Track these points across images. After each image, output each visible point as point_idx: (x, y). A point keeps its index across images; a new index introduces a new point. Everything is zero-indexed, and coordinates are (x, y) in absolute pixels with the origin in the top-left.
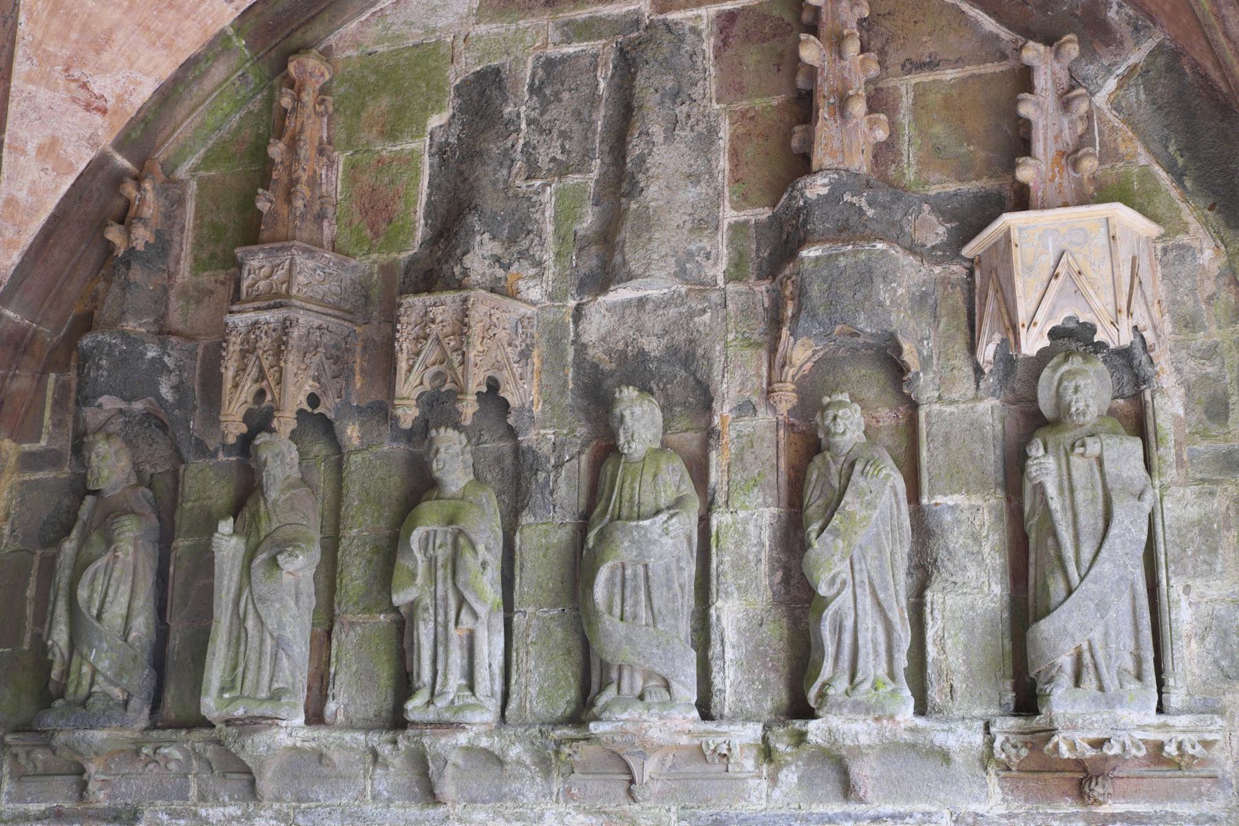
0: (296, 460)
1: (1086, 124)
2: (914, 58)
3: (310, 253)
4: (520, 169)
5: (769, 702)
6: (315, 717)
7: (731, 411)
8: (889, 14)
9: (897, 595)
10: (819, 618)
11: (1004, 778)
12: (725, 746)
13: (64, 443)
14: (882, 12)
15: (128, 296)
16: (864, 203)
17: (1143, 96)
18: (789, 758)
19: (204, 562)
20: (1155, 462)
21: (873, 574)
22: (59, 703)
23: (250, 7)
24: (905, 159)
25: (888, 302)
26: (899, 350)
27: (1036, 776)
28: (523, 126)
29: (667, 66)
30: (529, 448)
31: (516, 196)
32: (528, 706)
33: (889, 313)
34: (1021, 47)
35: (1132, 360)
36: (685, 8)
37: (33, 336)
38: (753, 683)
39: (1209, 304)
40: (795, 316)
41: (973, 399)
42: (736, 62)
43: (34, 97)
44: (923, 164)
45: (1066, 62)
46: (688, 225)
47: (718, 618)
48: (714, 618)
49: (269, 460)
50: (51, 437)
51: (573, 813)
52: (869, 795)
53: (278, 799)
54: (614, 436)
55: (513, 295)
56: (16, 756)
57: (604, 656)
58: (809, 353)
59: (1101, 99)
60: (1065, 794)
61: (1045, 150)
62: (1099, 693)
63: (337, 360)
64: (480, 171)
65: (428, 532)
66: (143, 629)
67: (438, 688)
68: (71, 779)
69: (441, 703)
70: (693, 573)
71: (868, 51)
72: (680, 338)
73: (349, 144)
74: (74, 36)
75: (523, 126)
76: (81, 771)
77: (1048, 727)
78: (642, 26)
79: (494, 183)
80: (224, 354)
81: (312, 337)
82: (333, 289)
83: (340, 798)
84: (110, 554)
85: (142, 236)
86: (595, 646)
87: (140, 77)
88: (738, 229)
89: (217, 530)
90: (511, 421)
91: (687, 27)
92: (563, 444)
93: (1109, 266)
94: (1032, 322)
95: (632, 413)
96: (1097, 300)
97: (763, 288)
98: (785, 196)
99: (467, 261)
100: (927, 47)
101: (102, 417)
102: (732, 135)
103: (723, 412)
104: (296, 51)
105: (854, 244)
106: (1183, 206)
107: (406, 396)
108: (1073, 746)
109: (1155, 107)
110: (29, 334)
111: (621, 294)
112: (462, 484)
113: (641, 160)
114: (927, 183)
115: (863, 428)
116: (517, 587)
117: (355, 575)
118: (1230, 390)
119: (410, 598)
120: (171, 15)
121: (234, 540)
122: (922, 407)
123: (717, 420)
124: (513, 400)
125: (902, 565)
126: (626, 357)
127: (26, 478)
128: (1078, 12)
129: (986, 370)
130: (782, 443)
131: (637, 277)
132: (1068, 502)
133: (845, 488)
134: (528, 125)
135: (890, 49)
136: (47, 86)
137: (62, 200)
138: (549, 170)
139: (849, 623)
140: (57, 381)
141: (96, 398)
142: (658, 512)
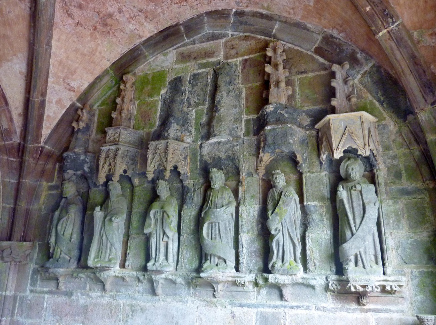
0: (120, 189)
1: (352, 88)
2: (299, 70)
3: (126, 130)
4: (186, 105)
5: (257, 267)
6: (123, 266)
7: (245, 175)
8: (292, 58)
9: (297, 234)
10: (272, 241)
11: (333, 295)
12: (243, 282)
13: (59, 183)
14: (290, 58)
15: (77, 142)
16: (284, 113)
17: (369, 80)
18: (263, 286)
19: (92, 218)
20: (378, 192)
21: (289, 227)
22: (51, 260)
23: (114, 62)
24: (297, 99)
25: (292, 142)
26: (296, 157)
27: (343, 295)
28: (187, 93)
29: (227, 75)
30: (186, 186)
31: (184, 112)
32: (184, 265)
33: (293, 146)
34: (331, 66)
35: (370, 159)
36: (233, 59)
37: (53, 152)
38: (252, 261)
39: (393, 142)
40: (264, 147)
41: (320, 172)
42: (247, 73)
43: (55, 88)
44: (303, 101)
45: (345, 70)
46: (233, 120)
47: (241, 239)
48: (240, 239)
49: (112, 189)
50: (56, 181)
51: (197, 301)
52: (289, 299)
53: (111, 291)
54: (210, 183)
55: (182, 141)
56: (41, 274)
57: (206, 252)
58: (269, 157)
59: (356, 81)
60: (353, 301)
61: (340, 96)
62: (364, 269)
63: (133, 160)
64: (174, 106)
65: (155, 212)
66: (75, 238)
67: (157, 259)
68: (55, 281)
69: (157, 264)
70: (234, 225)
71: (286, 69)
72: (230, 153)
73: (139, 99)
74: (65, 71)
75: (187, 93)
76: (57, 280)
77: (347, 280)
78: (221, 64)
79: (178, 109)
80: (100, 158)
81: (125, 153)
82: (132, 139)
83: (129, 292)
84: (67, 216)
85: (82, 125)
86: (203, 248)
87: (84, 82)
88: (247, 121)
89: (95, 210)
90: (181, 178)
91: (233, 64)
92: (196, 185)
93: (362, 131)
94: (337, 148)
95: (215, 176)
96: (358, 142)
97: (255, 138)
98: (261, 111)
99: (170, 131)
100: (303, 67)
101: (70, 176)
102: (246, 94)
103: (243, 175)
104: (126, 74)
105: (281, 125)
106: (384, 112)
107: (150, 171)
108: (355, 287)
109: (373, 83)
110: (52, 153)
111: (213, 140)
112: (166, 197)
113: (219, 101)
114: (303, 106)
115: (285, 181)
116: (182, 228)
117: (135, 223)
118: (402, 169)
119: (149, 231)
120: (92, 65)
121: (100, 213)
122: (303, 174)
123: (241, 178)
124: (182, 172)
125: (298, 224)
126: (215, 159)
127: (49, 193)
128: (349, 56)
129: (323, 163)
130: (260, 185)
131: (217, 135)
132: (351, 205)
133: (279, 200)
134: (188, 92)
135: (292, 68)
136: (58, 85)
137: (62, 115)
138: (194, 105)
139: (281, 243)
140: (59, 165)
141: (67, 170)
142: (223, 206)
